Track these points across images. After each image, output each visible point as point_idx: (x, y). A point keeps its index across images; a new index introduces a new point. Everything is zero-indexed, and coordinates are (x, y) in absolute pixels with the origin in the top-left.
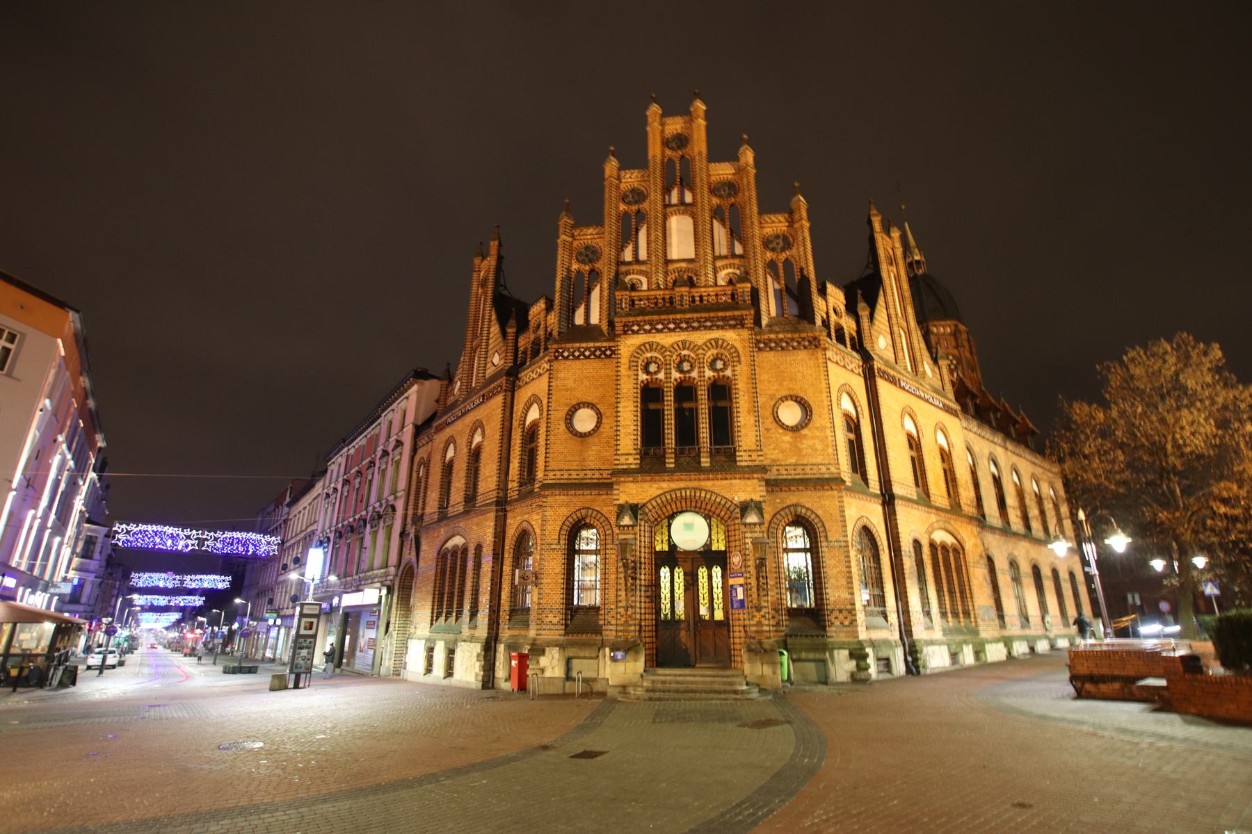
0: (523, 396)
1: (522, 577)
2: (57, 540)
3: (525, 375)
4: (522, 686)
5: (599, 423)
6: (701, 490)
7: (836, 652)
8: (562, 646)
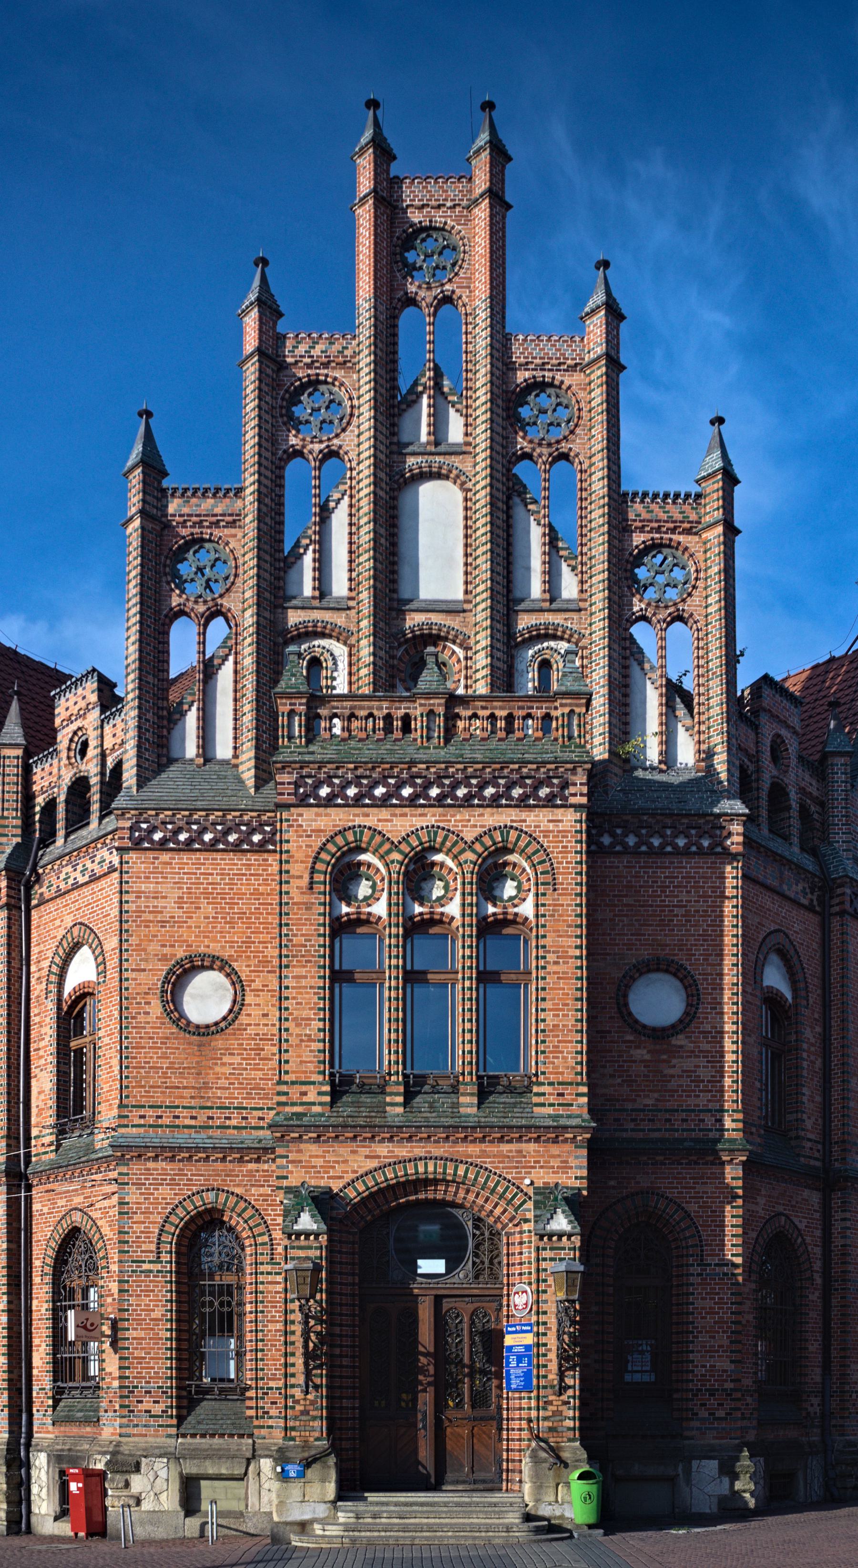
0: (49, 926)
1: (87, 1328)
2: (842, 701)
3: (55, 877)
4: (207, 761)
5: (232, 975)
6: (457, 1162)
7: (695, 1463)
8: (174, 1457)
